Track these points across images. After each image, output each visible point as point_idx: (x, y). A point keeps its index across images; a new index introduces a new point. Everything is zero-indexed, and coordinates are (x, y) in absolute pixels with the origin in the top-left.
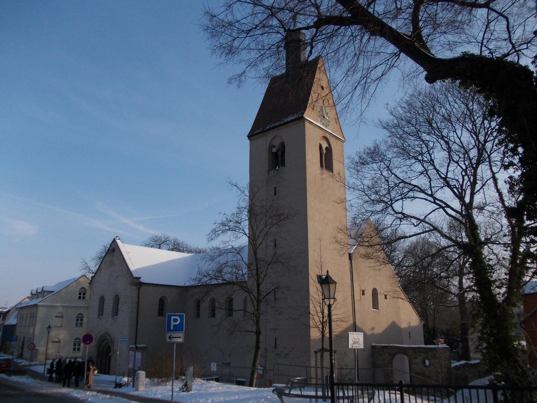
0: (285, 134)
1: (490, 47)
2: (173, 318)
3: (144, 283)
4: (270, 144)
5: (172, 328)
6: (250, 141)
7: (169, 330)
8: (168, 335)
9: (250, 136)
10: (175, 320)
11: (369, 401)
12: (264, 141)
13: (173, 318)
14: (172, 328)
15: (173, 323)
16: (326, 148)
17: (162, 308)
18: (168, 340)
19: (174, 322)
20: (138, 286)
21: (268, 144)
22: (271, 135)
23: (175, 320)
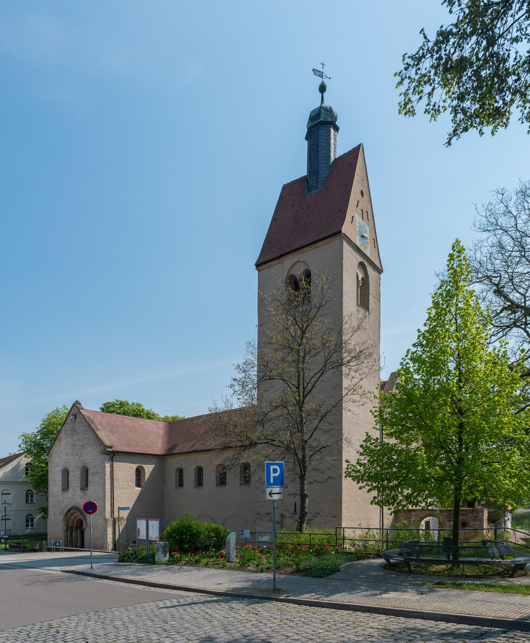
0: (313, 258)
1: (384, 439)
2: (272, 467)
3: (117, 452)
4: (288, 273)
5: (272, 482)
6: (259, 271)
7: (269, 484)
8: (268, 490)
9: (258, 265)
10: (275, 471)
11: (529, 36)
12: (281, 270)
13: (272, 467)
14: (272, 482)
15: (272, 475)
16: (363, 279)
17: (40, 549)
18: (268, 497)
19: (273, 473)
20: (112, 456)
21: (285, 275)
22: (289, 261)
23: (275, 471)
